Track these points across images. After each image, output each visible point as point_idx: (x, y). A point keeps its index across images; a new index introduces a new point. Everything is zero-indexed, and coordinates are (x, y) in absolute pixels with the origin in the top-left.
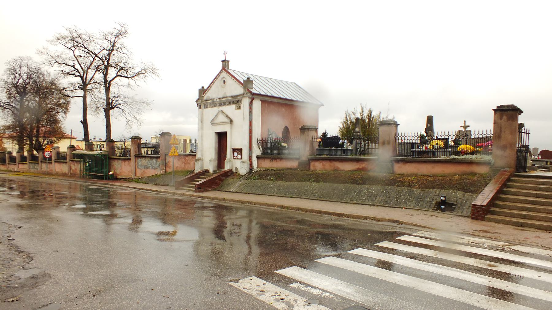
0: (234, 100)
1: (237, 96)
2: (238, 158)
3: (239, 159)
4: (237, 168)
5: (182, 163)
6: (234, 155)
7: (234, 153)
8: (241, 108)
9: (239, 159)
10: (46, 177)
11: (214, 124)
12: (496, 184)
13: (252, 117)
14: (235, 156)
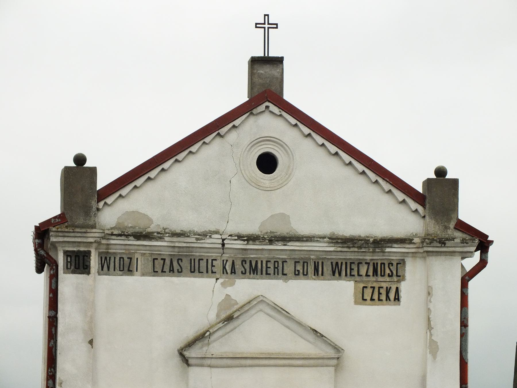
8: (397, 299)
11: (208, 362)
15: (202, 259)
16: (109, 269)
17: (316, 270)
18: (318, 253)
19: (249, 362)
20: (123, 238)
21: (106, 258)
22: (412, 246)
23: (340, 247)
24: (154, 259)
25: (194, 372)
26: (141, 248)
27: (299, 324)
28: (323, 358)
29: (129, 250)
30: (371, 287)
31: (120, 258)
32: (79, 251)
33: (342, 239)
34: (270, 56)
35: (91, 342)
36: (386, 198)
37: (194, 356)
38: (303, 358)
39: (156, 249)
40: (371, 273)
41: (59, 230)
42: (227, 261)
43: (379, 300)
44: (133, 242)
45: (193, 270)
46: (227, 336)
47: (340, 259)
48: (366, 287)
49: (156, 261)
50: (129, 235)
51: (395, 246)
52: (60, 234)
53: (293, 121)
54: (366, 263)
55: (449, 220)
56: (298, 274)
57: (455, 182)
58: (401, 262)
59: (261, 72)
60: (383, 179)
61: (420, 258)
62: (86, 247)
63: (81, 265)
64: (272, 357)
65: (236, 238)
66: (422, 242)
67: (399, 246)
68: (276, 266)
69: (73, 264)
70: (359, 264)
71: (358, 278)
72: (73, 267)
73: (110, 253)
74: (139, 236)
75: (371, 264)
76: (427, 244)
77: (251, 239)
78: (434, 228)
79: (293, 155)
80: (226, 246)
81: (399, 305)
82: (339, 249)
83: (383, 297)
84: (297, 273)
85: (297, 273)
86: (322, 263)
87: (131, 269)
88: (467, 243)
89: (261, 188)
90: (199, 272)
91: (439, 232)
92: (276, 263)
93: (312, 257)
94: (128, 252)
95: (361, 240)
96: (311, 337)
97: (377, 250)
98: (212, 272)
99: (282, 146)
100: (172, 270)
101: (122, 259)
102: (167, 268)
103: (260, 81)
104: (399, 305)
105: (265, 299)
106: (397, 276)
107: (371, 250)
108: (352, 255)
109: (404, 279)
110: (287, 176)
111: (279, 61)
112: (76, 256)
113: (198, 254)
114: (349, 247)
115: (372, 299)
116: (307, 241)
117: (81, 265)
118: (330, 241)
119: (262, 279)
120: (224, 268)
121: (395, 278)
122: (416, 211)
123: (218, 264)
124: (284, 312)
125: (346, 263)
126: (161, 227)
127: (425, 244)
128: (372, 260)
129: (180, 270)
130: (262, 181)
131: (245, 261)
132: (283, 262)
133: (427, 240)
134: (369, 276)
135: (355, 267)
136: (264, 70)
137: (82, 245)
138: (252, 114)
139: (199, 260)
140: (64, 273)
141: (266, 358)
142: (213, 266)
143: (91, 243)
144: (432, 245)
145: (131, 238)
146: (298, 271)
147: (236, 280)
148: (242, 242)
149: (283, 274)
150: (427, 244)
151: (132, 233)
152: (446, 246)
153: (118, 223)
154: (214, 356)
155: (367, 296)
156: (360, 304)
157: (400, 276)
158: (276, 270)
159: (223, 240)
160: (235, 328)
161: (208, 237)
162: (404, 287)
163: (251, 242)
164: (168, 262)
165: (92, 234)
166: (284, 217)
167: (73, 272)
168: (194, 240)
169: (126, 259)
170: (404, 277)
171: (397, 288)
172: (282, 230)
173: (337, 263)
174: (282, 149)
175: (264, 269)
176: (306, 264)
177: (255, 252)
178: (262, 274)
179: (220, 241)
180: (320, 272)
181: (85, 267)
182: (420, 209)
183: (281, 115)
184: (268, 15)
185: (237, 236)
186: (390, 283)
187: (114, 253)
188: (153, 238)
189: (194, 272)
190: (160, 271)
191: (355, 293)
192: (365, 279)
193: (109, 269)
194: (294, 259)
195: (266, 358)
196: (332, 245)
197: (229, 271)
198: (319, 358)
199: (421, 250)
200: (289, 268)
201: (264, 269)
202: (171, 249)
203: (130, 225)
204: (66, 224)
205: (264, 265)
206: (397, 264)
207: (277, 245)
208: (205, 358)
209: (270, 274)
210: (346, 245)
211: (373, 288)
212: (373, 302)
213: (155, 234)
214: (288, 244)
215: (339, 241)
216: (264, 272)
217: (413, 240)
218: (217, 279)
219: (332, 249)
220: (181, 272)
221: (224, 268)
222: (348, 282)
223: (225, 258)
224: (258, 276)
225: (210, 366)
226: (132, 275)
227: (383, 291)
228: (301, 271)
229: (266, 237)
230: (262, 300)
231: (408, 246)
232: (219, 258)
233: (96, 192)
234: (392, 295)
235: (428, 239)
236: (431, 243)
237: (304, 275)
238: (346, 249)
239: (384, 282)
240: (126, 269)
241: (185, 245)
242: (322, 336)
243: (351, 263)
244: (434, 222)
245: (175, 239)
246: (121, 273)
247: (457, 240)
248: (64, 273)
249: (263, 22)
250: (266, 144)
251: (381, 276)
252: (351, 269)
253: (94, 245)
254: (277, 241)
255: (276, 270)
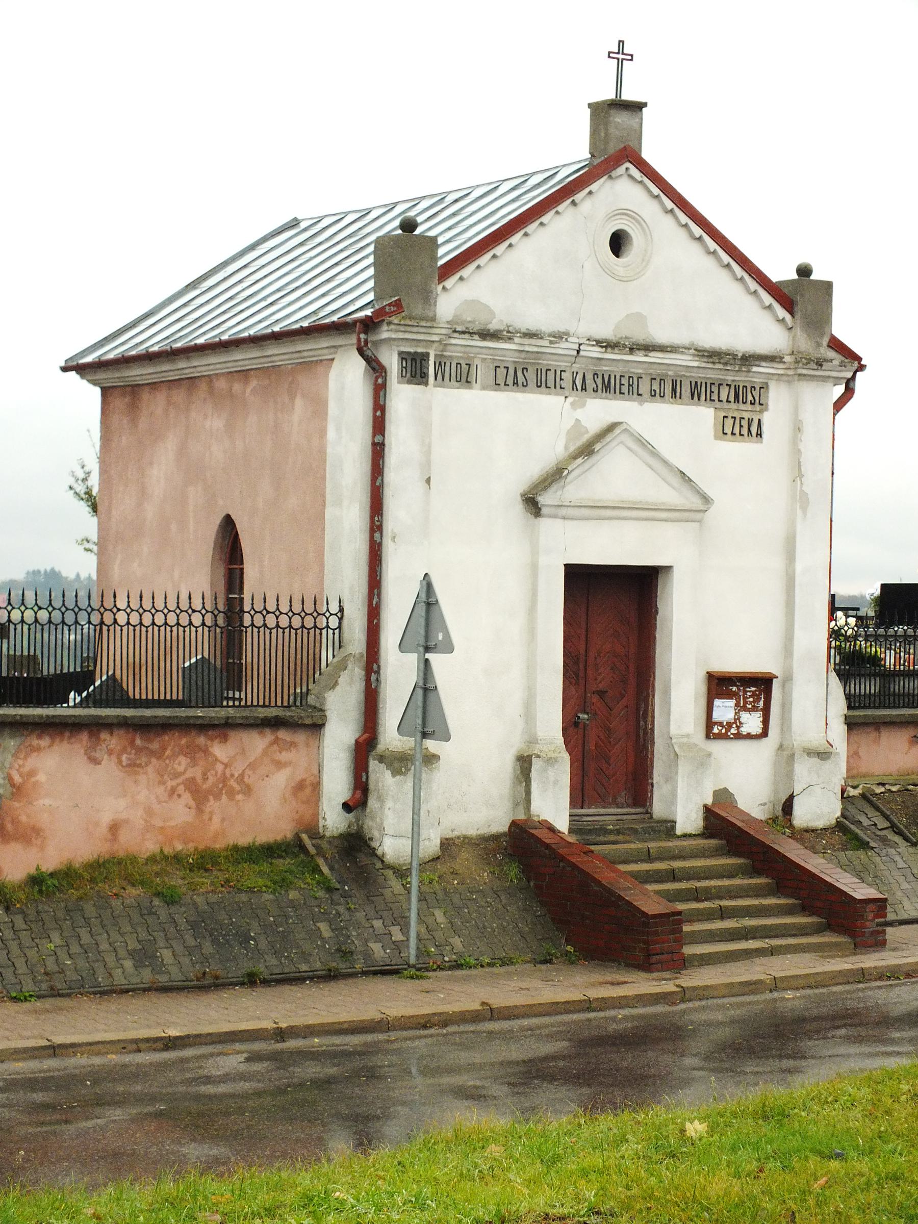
0: (713, 375)
1: (748, 360)
2: (744, 730)
3: (749, 736)
4: (725, 790)
5: (172, 792)
6: (717, 716)
7: (717, 702)
8: (759, 435)
9: (749, 736)
10: (175, 983)
11: (563, 512)
12: (139, 774)
13: (154, 308)
14: (720, 724)
15: (550, 370)
16: (699, 399)
17: (674, 390)
18: (678, 368)
19: (609, 513)
20: (467, 336)
21: (440, 363)
22: (781, 366)
23: (705, 362)
24: (496, 367)
25: (545, 524)
26: (484, 351)
27: (665, 462)
28: (690, 511)
29: (467, 353)
30: (732, 417)
31: (457, 364)
32: (416, 353)
33: (708, 352)
34: (623, 98)
35: (428, 481)
36: (749, 301)
37: (550, 503)
38: (669, 510)
39: (499, 352)
40: (732, 399)
41: (402, 322)
42: (577, 373)
43: (741, 435)
44: (477, 342)
45: (539, 384)
46: (582, 477)
47: (700, 377)
48: (727, 417)
49: (498, 369)
50: (474, 333)
51: (764, 364)
52: (402, 328)
53: (656, 191)
54: (727, 385)
55: (822, 335)
56: (655, 395)
57: (827, 288)
58: (764, 386)
59: (618, 120)
60: (750, 275)
61: (784, 381)
62: (425, 347)
63: (418, 372)
64: (637, 506)
65: (594, 343)
66: (797, 362)
67: (768, 365)
68: (631, 383)
69: (409, 370)
70: (720, 385)
71: (718, 404)
72: (408, 375)
73: (445, 357)
74: (486, 335)
75: (733, 387)
76: (803, 364)
77: (609, 345)
78: (804, 344)
79: (651, 236)
80: (582, 353)
81: (762, 442)
82: (703, 365)
83: (745, 431)
84: (653, 393)
85: (653, 393)
86: (681, 381)
87: (469, 380)
88: (845, 366)
89: (617, 278)
90: (547, 387)
91: (810, 350)
92: (631, 379)
93: (670, 373)
94: (466, 356)
95: (729, 354)
96: (676, 481)
97: (743, 369)
98: (561, 388)
99: (634, 218)
100: (516, 383)
101: (459, 366)
102: (510, 380)
103: (617, 133)
104: (762, 442)
105: (628, 428)
106: (760, 404)
107: (737, 369)
108: (713, 373)
109: (767, 409)
110: (644, 263)
111: (638, 107)
112: (412, 360)
113: (545, 362)
114: (714, 363)
115: (733, 434)
116: (671, 351)
117: (418, 372)
118: (696, 353)
119: (615, 399)
120: (574, 382)
121: (757, 407)
122: (783, 320)
123: (567, 376)
124: (649, 446)
125: (706, 383)
126: (505, 324)
127: (800, 365)
128: (733, 381)
129: (525, 384)
130: (616, 267)
131: (597, 375)
132: (638, 378)
133: (803, 360)
134: (730, 402)
135: (715, 389)
136: (621, 118)
137: (422, 344)
138: (610, 177)
139: (547, 370)
140: (398, 383)
141: (629, 508)
142: (561, 379)
143: (433, 342)
144: (809, 366)
145: (476, 337)
146: (654, 390)
147: (588, 400)
148: (599, 349)
149: (639, 395)
150: (803, 364)
151: (478, 330)
152: (823, 368)
153: (455, 316)
154: (572, 504)
155: (728, 430)
156: (721, 439)
157: (762, 405)
158: (631, 388)
159: (580, 345)
160: (593, 465)
161: (564, 340)
162: (767, 418)
163: (609, 350)
164: (511, 371)
165: (438, 329)
166: (640, 318)
167: (409, 382)
168: (546, 343)
169: (463, 365)
170: (767, 405)
171: (759, 420)
172: (639, 336)
173: (696, 383)
174: (638, 226)
175: (618, 387)
176: (662, 382)
177: (610, 363)
178: (615, 393)
179: (576, 347)
180: (678, 394)
181: (423, 375)
182: (788, 317)
183: (641, 182)
184: (623, 42)
185: (596, 341)
186: (752, 413)
187: (450, 357)
188: (502, 339)
189: (540, 386)
190: (502, 384)
191: (715, 424)
192: (726, 405)
193: (699, 399)
194: (650, 374)
195: (629, 508)
196: (697, 359)
197: (579, 387)
198: (684, 510)
199: (790, 372)
200: (645, 388)
201: (618, 387)
202: (517, 354)
203: (469, 319)
204: (403, 314)
205: (618, 381)
206: (760, 388)
207: (637, 355)
208: (561, 506)
209: (623, 393)
210: (711, 360)
211: (734, 418)
212: (734, 437)
213: (505, 333)
214: (650, 354)
215: (706, 354)
216: (618, 391)
217: (783, 358)
218: (566, 397)
219: (696, 364)
220: (526, 386)
221: (574, 382)
222: (708, 409)
223: (575, 370)
224: (611, 396)
225: (564, 518)
226: (471, 388)
227: (745, 423)
228: (658, 391)
229: (627, 343)
230: (626, 429)
231: (776, 365)
232: (568, 368)
233: (437, 270)
234: (754, 430)
235: (806, 359)
236: (807, 363)
237: (661, 396)
238: (710, 366)
239: (745, 411)
240: (464, 379)
241: (536, 349)
242: (691, 480)
243: (711, 384)
244: (805, 335)
245: (527, 341)
246: (458, 384)
247: (836, 362)
248: (398, 383)
249: (617, 51)
250: (621, 219)
251: (743, 403)
252: (711, 392)
253: (436, 345)
254: (638, 349)
255: (631, 388)
